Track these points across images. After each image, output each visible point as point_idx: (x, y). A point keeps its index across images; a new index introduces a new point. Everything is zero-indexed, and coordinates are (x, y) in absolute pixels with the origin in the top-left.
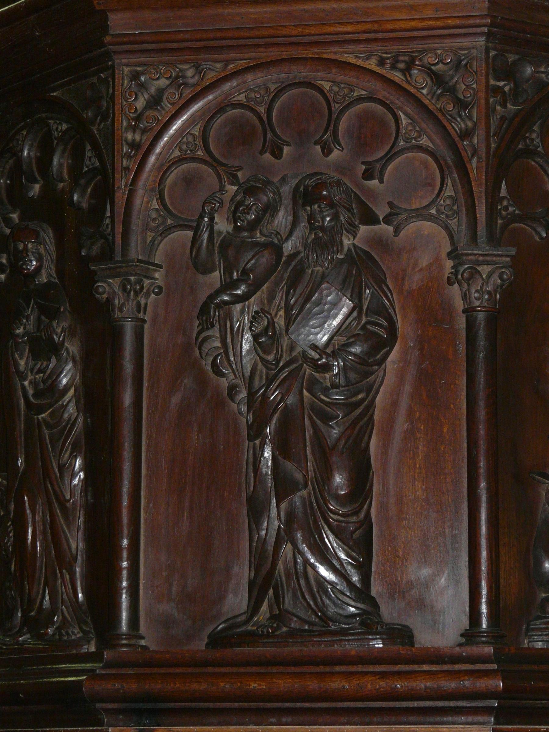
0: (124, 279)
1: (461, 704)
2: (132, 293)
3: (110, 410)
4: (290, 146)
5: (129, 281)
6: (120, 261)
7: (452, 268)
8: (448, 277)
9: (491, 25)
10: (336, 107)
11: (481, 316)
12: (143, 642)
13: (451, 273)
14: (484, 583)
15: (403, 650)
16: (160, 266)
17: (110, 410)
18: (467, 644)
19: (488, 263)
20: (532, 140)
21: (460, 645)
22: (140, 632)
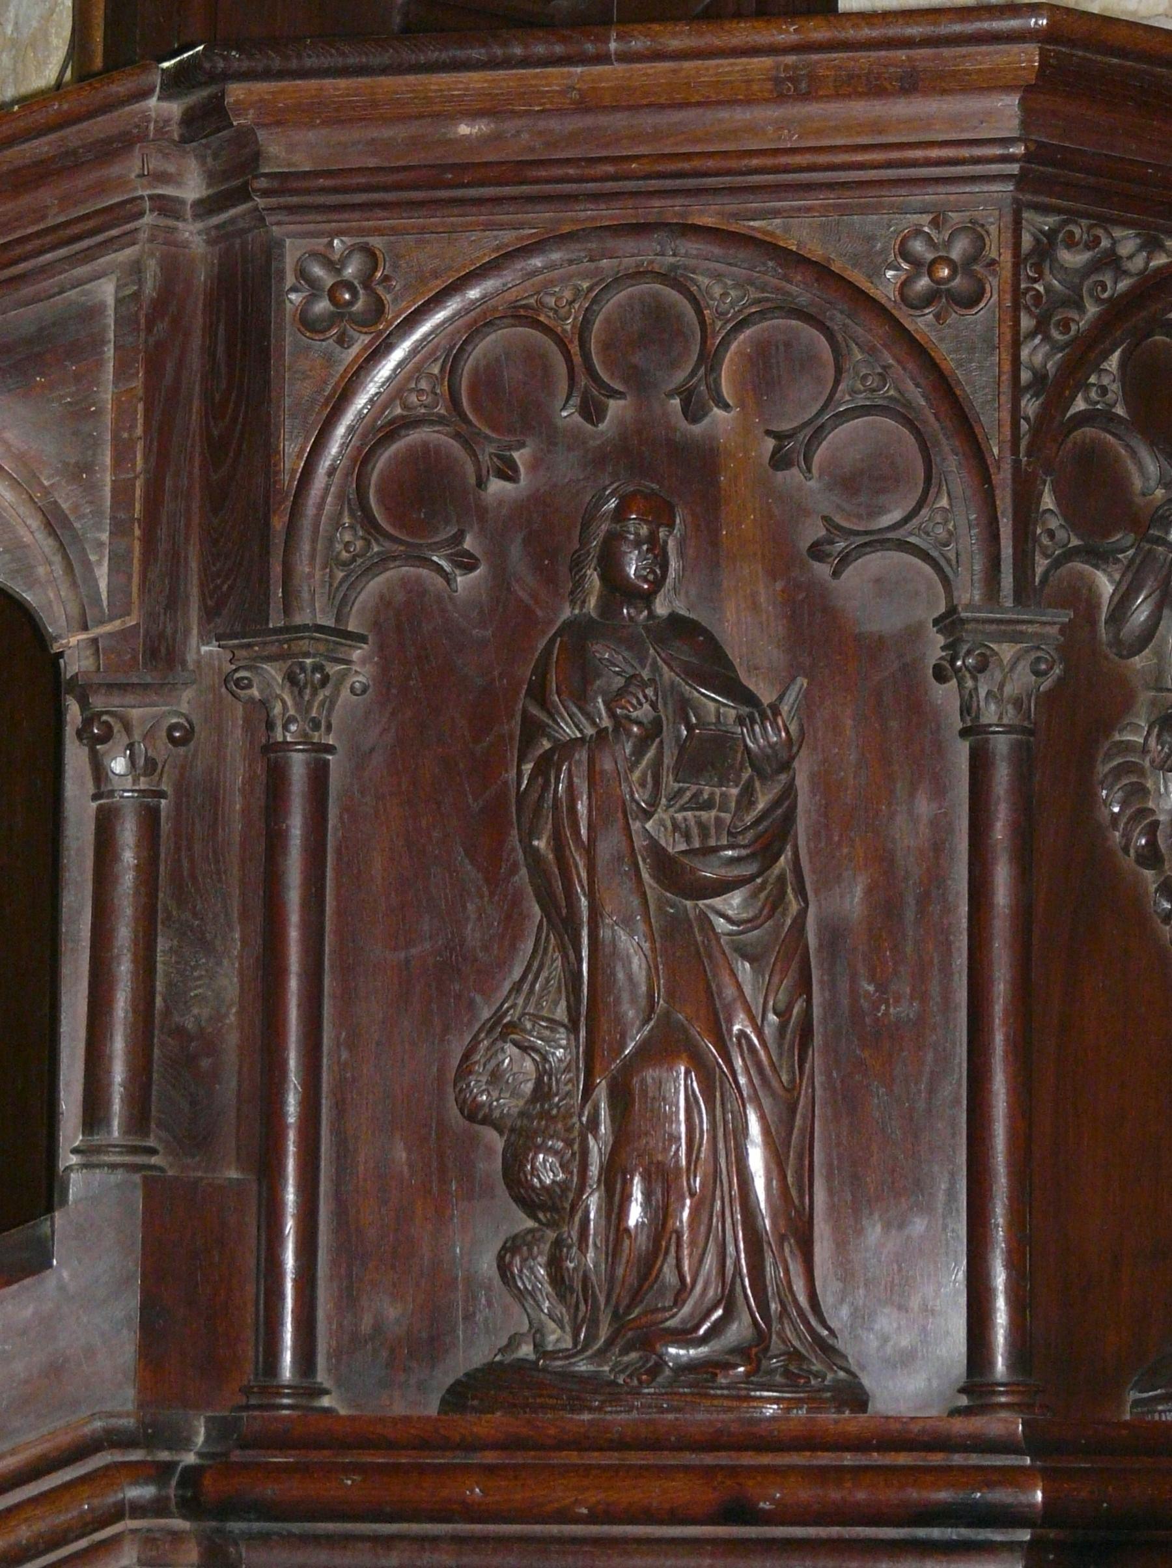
0: (293, 663)
1: (936, 1533)
2: (308, 691)
3: (618, 1186)
4: (625, 399)
5: (303, 668)
6: (966, 1407)
7: (943, 648)
8: (935, 667)
9: (1027, 158)
10: (720, 329)
11: (1001, 744)
12: (326, 1402)
13: (942, 658)
14: (1001, 1303)
15: (831, 1419)
16: (362, 639)
17: (618, 1186)
18: (966, 1412)
19: (1014, 638)
20: (1104, 391)
21: (956, 1412)
22: (319, 1380)
